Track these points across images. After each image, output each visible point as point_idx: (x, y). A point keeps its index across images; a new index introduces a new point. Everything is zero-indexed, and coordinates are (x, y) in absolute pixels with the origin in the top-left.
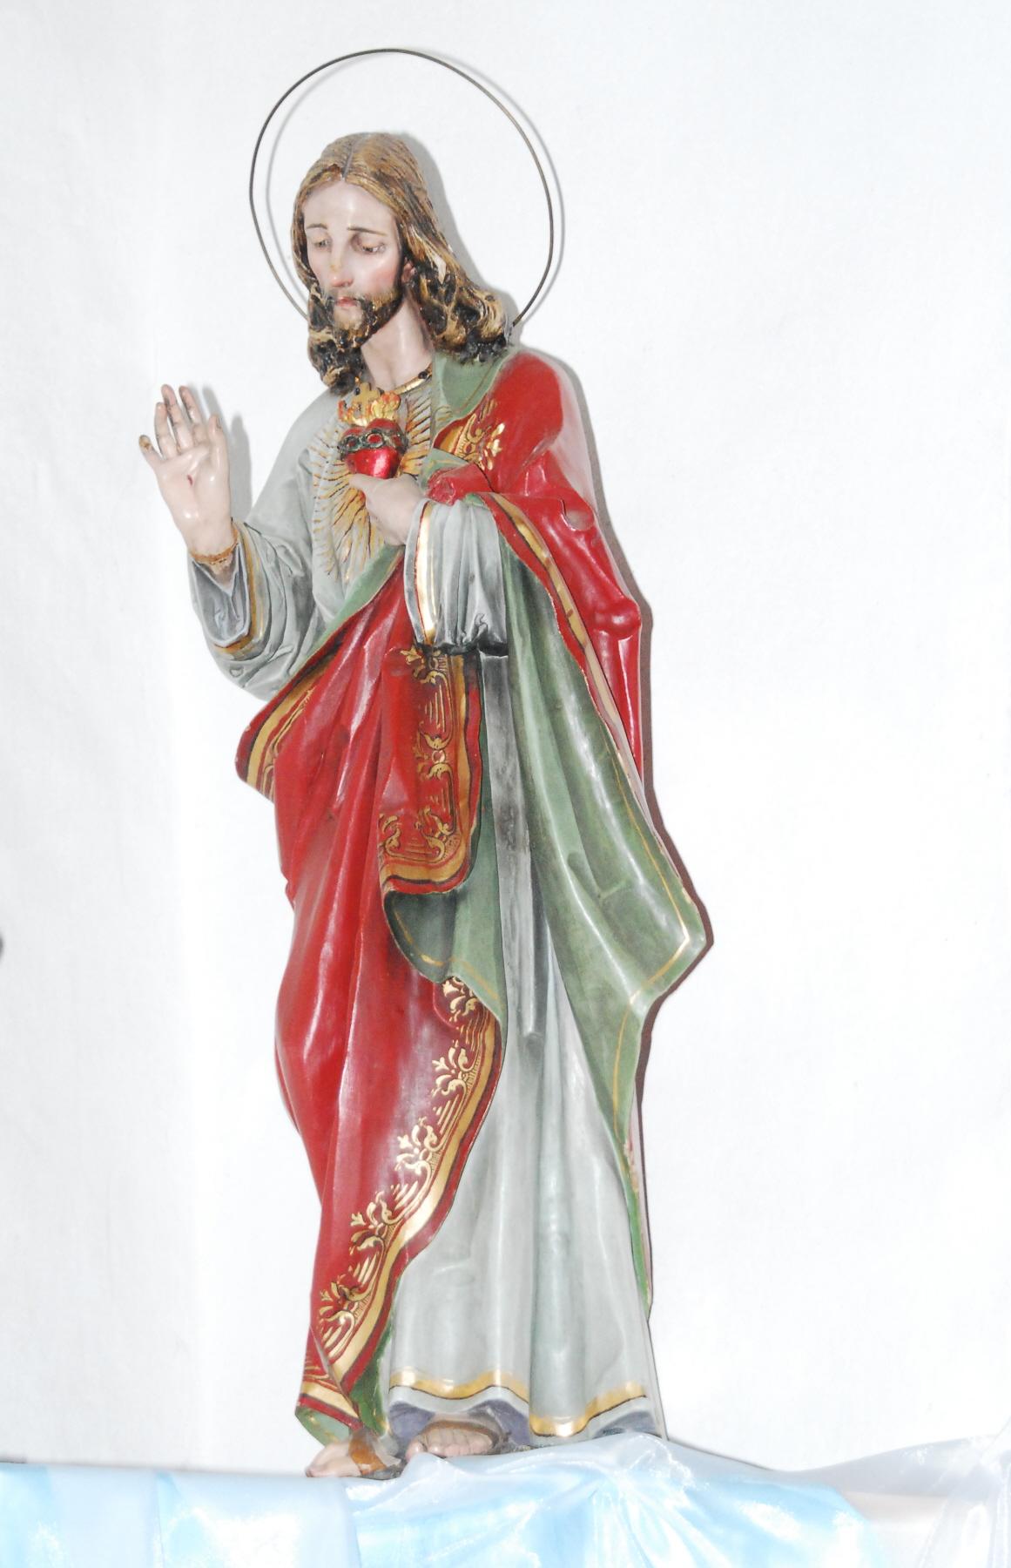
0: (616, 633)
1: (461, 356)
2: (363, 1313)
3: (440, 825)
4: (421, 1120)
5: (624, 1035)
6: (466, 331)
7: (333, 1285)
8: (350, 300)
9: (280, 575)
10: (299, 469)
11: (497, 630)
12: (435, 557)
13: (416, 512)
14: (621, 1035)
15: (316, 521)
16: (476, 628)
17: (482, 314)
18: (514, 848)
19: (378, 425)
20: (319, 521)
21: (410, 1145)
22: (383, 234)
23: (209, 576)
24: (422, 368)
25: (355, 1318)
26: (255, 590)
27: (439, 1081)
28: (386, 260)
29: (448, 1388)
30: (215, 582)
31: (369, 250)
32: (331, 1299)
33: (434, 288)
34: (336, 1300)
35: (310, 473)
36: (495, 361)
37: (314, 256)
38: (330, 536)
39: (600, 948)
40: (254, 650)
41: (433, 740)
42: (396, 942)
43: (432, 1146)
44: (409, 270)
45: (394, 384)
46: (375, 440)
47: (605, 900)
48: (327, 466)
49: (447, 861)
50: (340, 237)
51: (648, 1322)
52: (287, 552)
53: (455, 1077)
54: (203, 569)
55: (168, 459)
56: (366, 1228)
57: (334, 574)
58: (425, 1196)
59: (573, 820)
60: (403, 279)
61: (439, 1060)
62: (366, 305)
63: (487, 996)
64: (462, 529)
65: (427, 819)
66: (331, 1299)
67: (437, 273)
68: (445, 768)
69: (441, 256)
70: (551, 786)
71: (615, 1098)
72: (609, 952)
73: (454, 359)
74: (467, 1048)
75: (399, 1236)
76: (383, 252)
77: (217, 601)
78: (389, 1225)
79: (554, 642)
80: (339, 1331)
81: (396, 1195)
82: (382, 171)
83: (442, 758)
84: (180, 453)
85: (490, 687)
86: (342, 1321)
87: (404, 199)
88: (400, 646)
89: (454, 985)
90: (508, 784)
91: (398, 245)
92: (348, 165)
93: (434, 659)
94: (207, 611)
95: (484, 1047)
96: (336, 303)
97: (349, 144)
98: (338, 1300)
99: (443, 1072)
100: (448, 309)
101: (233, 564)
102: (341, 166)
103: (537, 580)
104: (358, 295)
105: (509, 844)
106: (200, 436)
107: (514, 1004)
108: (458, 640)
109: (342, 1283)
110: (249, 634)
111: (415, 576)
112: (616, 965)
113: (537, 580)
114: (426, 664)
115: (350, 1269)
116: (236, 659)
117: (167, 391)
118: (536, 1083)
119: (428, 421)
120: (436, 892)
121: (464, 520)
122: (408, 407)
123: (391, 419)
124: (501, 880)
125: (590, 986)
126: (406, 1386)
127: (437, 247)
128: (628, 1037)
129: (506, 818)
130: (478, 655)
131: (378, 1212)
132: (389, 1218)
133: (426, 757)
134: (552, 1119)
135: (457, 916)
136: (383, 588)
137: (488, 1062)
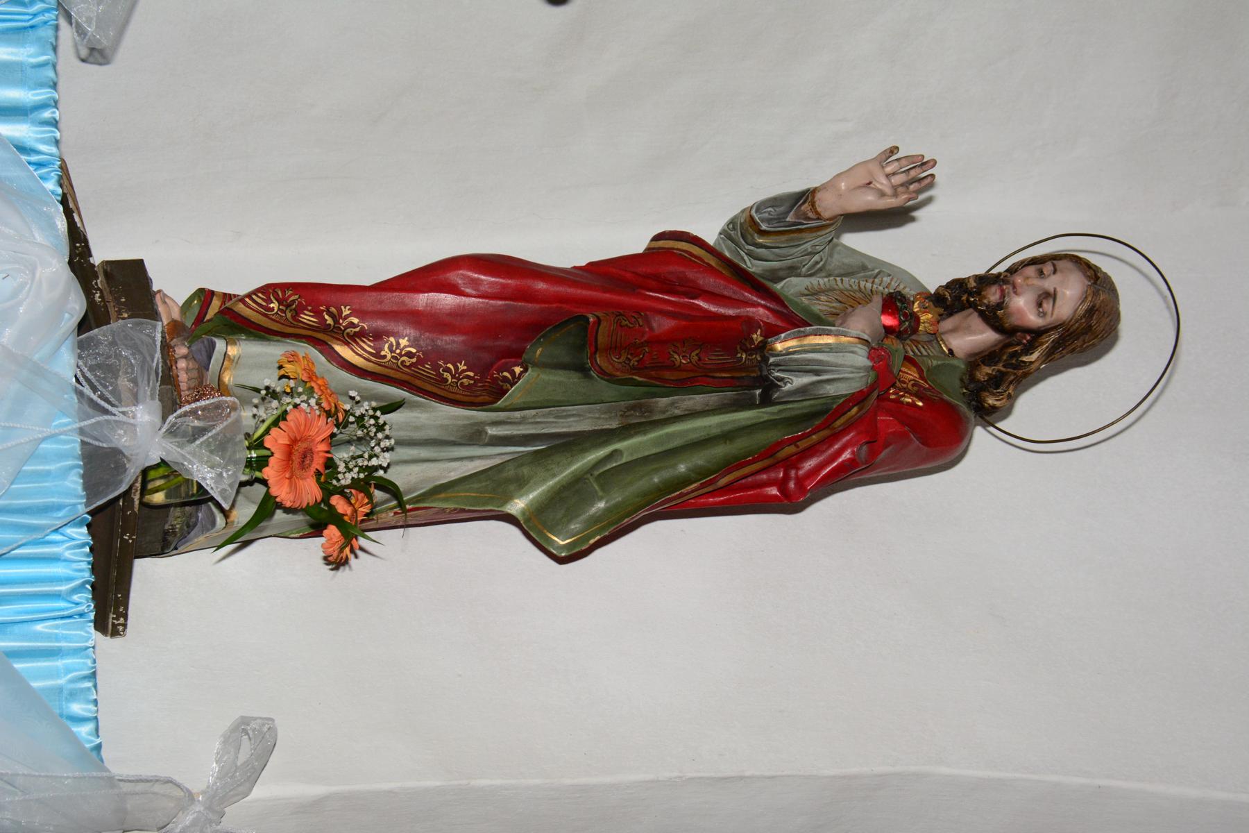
0: (782, 484)
1: (966, 378)
2: (277, 319)
3: (637, 359)
4: (421, 354)
5: (490, 497)
6: (984, 381)
7: (297, 297)
8: (1003, 296)
9: (802, 256)
10: (877, 271)
11: (782, 395)
12: (831, 349)
13: (861, 333)
14: (490, 495)
15: (842, 280)
16: (781, 379)
17: (998, 391)
18: (621, 416)
19: (915, 319)
20: (842, 283)
21: (402, 346)
22: (1052, 314)
23: (799, 203)
24: (955, 350)
25: (273, 315)
26: (792, 235)
27: (450, 365)
28: (1033, 319)
29: (227, 378)
30: (795, 208)
31: (1040, 305)
32: (287, 296)
33: (1015, 355)
34: (286, 300)
35: (875, 278)
36: (965, 402)
37: (1031, 271)
38: (832, 290)
39: (554, 476)
40: (749, 236)
41: (697, 355)
42: (551, 327)
43: (403, 361)
44: (1025, 339)
45: (943, 333)
46: (905, 315)
47: (588, 479)
48: (881, 288)
49: (612, 364)
50: (1049, 284)
51: (275, 536)
52: (817, 263)
53: (453, 377)
54: (804, 198)
55: (883, 167)
56: (340, 317)
57: (806, 292)
58: (365, 358)
59: (647, 453)
60: (1019, 334)
61: (464, 365)
62: (1000, 305)
63: (514, 394)
64: (852, 366)
65: (640, 349)
66: (287, 296)
67: (1026, 355)
68: (677, 364)
69: (1038, 357)
70: (670, 436)
71: (443, 495)
72: (551, 483)
73: (964, 374)
74: (475, 385)
75: (335, 341)
76: (1039, 315)
77: (782, 209)
78: (343, 334)
79: (773, 436)
80: (264, 304)
81: (365, 337)
82: (1097, 312)
83: (684, 362)
84: (888, 176)
85: (736, 397)
86: (272, 305)
87: (1078, 328)
88: (763, 328)
89: (520, 374)
90: (667, 411)
91: (1044, 326)
92: (1100, 288)
93: (754, 356)
94: (774, 202)
95: (477, 396)
96: (1001, 286)
97: (1112, 289)
98: (286, 301)
99: (456, 368)
100: (1000, 367)
101: (810, 219)
102: (1098, 282)
103: (817, 422)
104: (1007, 299)
105: (625, 412)
106: (901, 189)
107: (509, 418)
108: (772, 367)
109: (299, 302)
110: (761, 231)
111: (816, 335)
112: (543, 488)
113: (817, 422)
114: (752, 349)
115: (310, 308)
116: (741, 224)
117: (932, 163)
118: (452, 439)
119: (919, 354)
120: (589, 355)
121: (859, 368)
122: (928, 342)
123: (920, 329)
124: (598, 406)
125: (526, 471)
126: (227, 349)
127: (1045, 355)
128: (490, 501)
129: (643, 410)
130: (758, 388)
131: (352, 325)
132: (348, 334)
133: (684, 349)
134: (423, 453)
135: (572, 372)
136: (803, 320)
137: (466, 399)
